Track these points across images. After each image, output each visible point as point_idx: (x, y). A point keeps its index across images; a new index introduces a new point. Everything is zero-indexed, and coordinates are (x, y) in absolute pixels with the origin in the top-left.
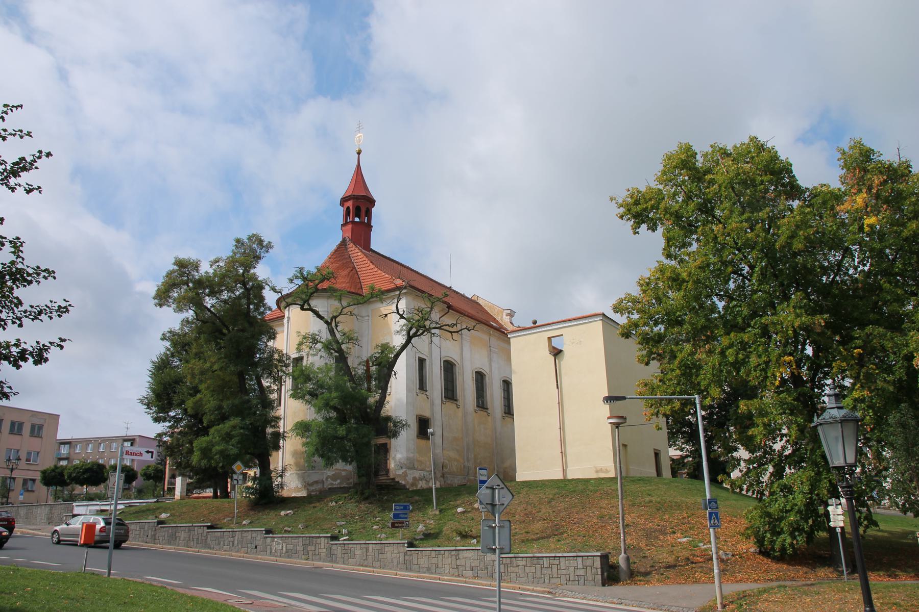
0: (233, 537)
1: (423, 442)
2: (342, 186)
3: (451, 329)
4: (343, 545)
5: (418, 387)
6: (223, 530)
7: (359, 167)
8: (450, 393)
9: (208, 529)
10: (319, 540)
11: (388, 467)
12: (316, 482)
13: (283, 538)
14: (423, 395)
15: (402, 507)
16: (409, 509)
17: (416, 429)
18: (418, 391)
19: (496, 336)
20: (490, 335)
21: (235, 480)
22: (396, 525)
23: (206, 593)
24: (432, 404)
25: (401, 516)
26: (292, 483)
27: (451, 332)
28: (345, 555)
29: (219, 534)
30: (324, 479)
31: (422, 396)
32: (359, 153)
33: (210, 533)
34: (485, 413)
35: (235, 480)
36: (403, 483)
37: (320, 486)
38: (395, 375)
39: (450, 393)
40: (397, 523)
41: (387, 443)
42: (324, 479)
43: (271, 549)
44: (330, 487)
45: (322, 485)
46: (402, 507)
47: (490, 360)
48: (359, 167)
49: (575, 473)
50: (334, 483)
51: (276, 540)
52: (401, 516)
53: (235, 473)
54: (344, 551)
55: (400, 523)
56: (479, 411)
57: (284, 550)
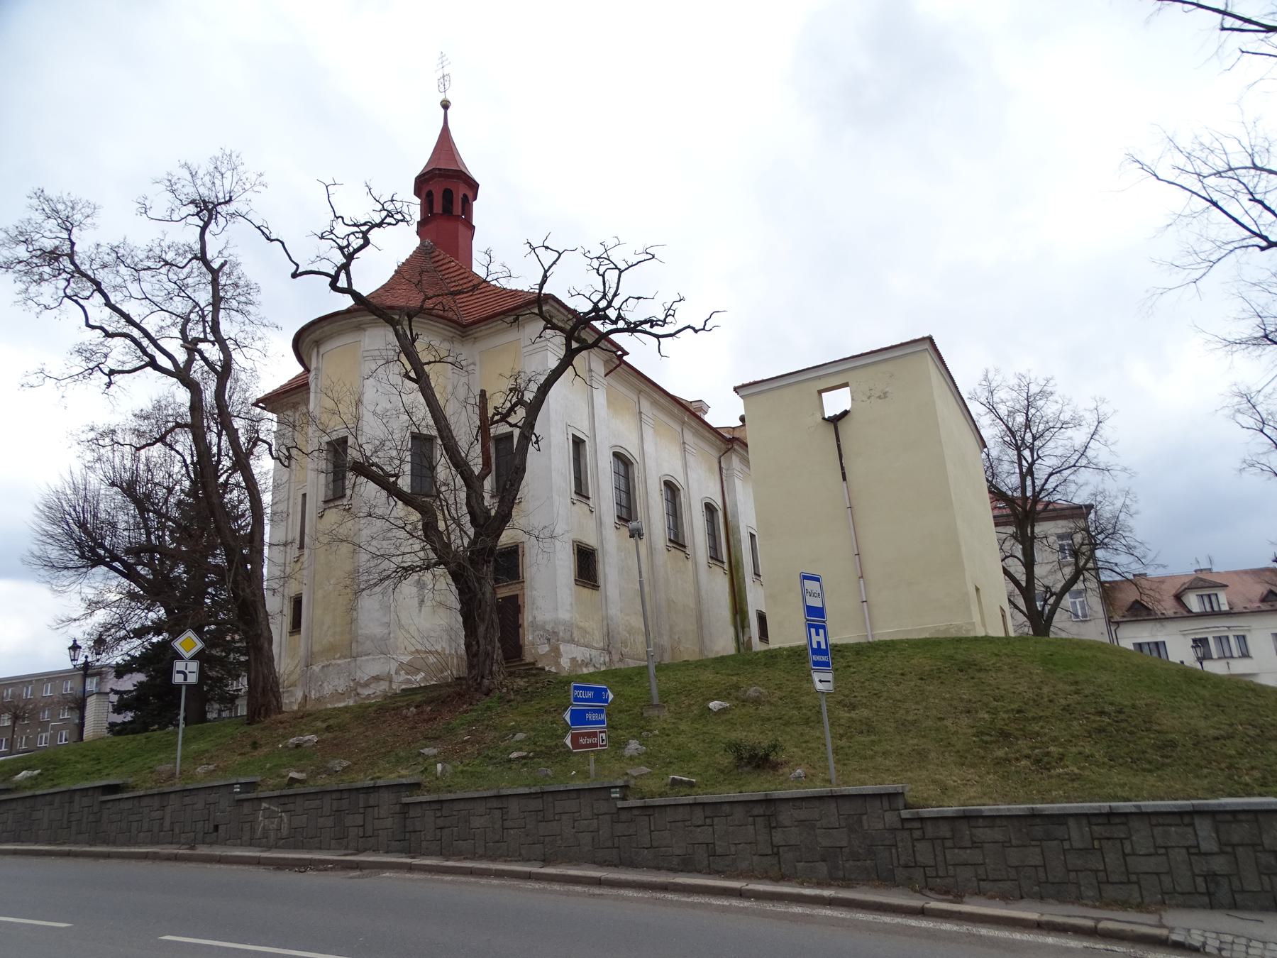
0: (162, 808)
1: (586, 592)
2: (419, 159)
3: (656, 330)
4: (438, 806)
5: (573, 489)
6: (137, 794)
7: (445, 131)
8: (627, 513)
9: (104, 794)
10: (373, 799)
11: (521, 642)
12: (377, 679)
13: (282, 800)
14: (583, 505)
15: (590, 694)
16: (606, 701)
17: (572, 566)
18: (574, 496)
19: (692, 427)
20: (683, 423)
21: (179, 672)
22: (582, 741)
23: (461, 806)
24: (600, 524)
25: (589, 716)
26: (325, 684)
27: (658, 337)
28: (446, 831)
29: (128, 805)
30: (393, 672)
31: (581, 508)
32: (446, 105)
33: (109, 805)
34: (683, 554)
35: (179, 672)
36: (553, 670)
37: (383, 686)
38: (537, 442)
39: (627, 513)
40: (583, 735)
41: (517, 596)
42: (393, 672)
43: (253, 830)
44: (403, 687)
45: (387, 683)
46: (590, 694)
47: (685, 466)
48: (445, 131)
49: (886, 630)
50: (412, 678)
51: (264, 805)
52: (589, 716)
53: (180, 658)
54: (440, 822)
55: (589, 735)
56: (673, 550)
57: (285, 832)
